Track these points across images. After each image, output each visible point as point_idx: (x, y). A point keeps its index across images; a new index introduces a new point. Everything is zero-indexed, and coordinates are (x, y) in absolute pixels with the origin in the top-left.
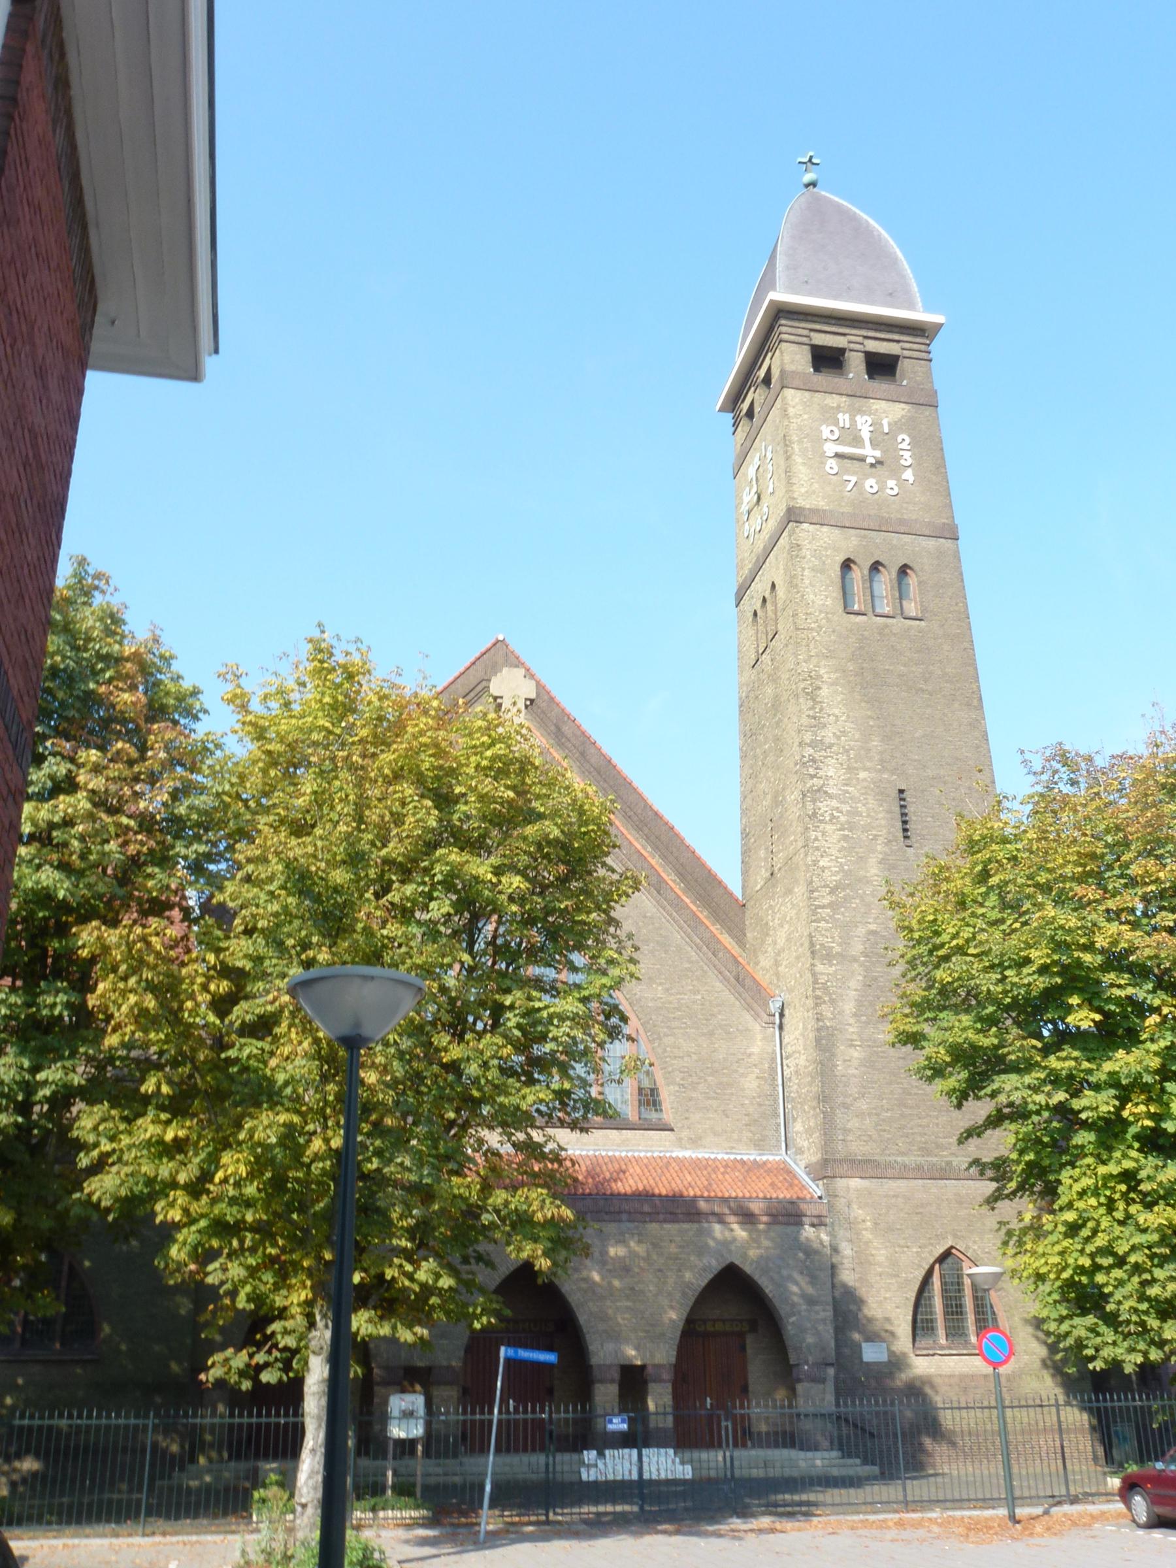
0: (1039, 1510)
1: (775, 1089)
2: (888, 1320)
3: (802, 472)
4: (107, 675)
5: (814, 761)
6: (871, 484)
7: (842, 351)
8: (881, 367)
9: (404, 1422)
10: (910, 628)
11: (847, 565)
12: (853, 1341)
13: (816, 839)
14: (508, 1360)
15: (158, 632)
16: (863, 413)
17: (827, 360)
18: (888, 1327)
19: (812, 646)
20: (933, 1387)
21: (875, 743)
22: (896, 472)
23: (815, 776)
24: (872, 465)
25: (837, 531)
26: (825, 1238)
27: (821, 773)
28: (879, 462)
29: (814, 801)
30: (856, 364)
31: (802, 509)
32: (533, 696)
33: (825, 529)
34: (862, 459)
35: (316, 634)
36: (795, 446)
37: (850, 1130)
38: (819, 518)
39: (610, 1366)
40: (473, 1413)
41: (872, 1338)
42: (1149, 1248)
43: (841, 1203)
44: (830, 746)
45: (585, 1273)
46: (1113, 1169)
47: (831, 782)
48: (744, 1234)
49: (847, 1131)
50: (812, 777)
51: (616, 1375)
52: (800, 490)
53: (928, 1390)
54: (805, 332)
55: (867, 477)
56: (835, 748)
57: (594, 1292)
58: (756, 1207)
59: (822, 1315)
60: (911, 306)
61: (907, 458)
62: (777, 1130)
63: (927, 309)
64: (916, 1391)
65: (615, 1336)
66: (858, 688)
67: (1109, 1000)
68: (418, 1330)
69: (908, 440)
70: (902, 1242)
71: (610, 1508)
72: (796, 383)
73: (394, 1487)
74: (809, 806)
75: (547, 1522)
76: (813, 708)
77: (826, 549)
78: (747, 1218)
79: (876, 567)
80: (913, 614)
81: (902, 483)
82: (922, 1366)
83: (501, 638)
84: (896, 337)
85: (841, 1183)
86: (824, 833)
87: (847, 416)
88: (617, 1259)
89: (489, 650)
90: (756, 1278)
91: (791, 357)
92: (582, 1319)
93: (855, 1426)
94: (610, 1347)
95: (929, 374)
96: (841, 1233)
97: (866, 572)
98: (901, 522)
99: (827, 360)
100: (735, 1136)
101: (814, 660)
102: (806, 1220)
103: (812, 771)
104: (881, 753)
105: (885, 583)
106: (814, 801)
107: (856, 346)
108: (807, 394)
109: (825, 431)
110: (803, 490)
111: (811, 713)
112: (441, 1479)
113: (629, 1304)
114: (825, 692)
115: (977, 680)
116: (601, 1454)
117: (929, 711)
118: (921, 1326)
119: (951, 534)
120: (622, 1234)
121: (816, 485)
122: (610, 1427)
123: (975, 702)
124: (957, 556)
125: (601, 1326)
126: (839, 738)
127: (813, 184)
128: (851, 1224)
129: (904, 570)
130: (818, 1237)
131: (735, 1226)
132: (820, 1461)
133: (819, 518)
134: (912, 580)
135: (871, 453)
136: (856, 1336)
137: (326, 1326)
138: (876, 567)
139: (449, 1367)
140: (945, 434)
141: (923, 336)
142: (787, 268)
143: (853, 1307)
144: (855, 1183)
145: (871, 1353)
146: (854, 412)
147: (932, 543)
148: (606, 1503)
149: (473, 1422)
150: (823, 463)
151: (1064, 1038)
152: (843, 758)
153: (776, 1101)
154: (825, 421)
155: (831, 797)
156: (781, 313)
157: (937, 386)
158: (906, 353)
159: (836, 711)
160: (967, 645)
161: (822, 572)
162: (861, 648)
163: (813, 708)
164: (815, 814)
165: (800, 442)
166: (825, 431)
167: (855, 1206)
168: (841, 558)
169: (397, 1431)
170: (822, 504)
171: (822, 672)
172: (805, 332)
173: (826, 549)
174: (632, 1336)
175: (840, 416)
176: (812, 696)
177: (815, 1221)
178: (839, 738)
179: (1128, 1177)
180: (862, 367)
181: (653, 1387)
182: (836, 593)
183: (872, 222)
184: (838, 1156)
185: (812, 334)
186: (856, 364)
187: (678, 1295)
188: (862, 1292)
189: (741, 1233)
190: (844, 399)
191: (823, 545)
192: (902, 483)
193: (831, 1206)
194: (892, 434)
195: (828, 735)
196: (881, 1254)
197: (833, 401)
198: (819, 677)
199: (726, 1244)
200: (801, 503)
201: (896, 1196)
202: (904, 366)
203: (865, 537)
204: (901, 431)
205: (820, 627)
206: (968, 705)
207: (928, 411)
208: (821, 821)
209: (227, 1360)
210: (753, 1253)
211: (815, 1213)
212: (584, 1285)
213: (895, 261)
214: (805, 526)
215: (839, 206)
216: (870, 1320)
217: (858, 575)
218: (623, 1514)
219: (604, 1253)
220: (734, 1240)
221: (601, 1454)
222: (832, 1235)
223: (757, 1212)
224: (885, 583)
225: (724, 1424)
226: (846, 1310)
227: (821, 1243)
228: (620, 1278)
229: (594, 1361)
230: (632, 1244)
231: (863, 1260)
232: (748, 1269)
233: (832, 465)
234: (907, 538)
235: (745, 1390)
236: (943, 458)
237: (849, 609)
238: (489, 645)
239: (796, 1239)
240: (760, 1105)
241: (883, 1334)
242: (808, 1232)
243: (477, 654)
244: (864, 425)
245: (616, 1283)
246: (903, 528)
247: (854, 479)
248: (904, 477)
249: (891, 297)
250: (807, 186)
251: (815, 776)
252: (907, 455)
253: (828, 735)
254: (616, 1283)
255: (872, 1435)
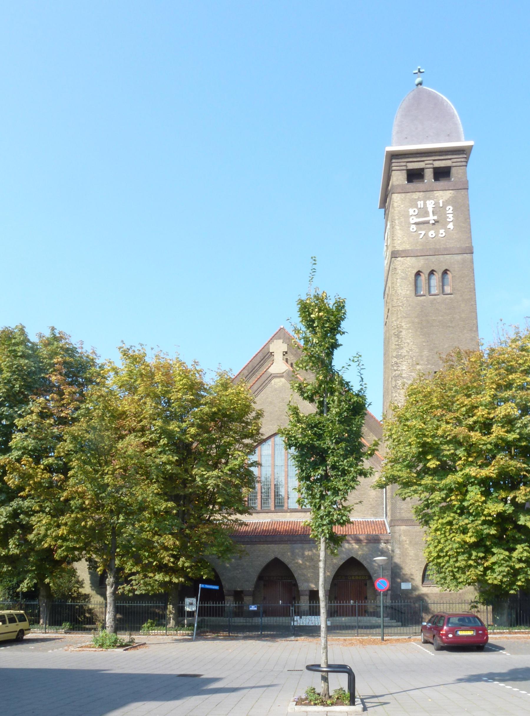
0: (407, 637)
1: (383, 494)
2: (412, 575)
3: (399, 233)
4: (50, 370)
5: (397, 364)
6: (432, 234)
7: (422, 170)
8: (442, 174)
9: (191, 606)
10: (446, 298)
11: (418, 274)
12: (397, 582)
13: (396, 396)
14: (201, 588)
15: (95, 349)
16: (429, 199)
17: (414, 176)
18: (412, 577)
19: (399, 313)
20: (428, 597)
21: (426, 353)
22: (444, 226)
23: (397, 370)
24: (433, 224)
25: (414, 259)
26: (390, 547)
27: (400, 368)
28: (436, 222)
29: (396, 381)
30: (429, 174)
31: (398, 251)
32: (286, 350)
33: (408, 258)
34: (428, 222)
35: (121, 345)
36: (397, 222)
37: (403, 509)
38: (405, 254)
39: (305, 591)
40: (205, 604)
41: (406, 581)
42: (456, 549)
43: (397, 535)
44: (405, 356)
45: (296, 561)
46: (444, 521)
47: (404, 372)
48: (357, 547)
49: (400, 509)
50: (395, 370)
51: (308, 593)
52: (397, 242)
53: (426, 598)
54: (404, 164)
55: (430, 230)
56: (407, 357)
57: (300, 567)
58: (361, 537)
59: (387, 573)
60: (459, 140)
61: (451, 217)
62: (383, 510)
63: (467, 139)
64: (421, 598)
65: (307, 581)
66: (419, 330)
67: (443, 456)
68: (180, 579)
69: (451, 208)
70: (421, 548)
71: (269, 633)
72: (399, 190)
73: (187, 625)
74: (394, 383)
75: (229, 636)
76: (397, 341)
77: (408, 268)
78: (358, 541)
79: (432, 272)
80: (449, 292)
81: (447, 230)
82: (424, 590)
83: (282, 327)
84: (449, 157)
85: (397, 528)
86: (399, 394)
87: (422, 202)
88: (308, 555)
89: (277, 332)
90: (361, 561)
91: (399, 178)
92: (296, 576)
93: (398, 611)
94: (306, 584)
95: (465, 173)
96: (396, 546)
97: (427, 276)
98: (446, 249)
99: (414, 176)
100: (366, 512)
101: (400, 320)
102: (382, 541)
103: (395, 368)
104: (428, 357)
105: (435, 280)
106: (396, 381)
107: (428, 165)
108: (403, 195)
109: (411, 211)
110: (399, 242)
111: (397, 343)
112: (245, 624)
113: (312, 571)
114: (404, 333)
115: (476, 318)
116: (301, 618)
117: (452, 335)
118: (424, 577)
119: (470, 251)
120: (311, 548)
121: (406, 239)
122: (251, 609)
123: (475, 329)
124: (472, 262)
125: (303, 578)
126: (408, 352)
127: (420, 84)
128: (400, 542)
129: (445, 272)
130: (387, 547)
131: (354, 544)
132: (379, 621)
133: (405, 254)
134: (450, 276)
135: (432, 218)
136: (399, 580)
137: (111, 578)
138: (432, 272)
139: (249, 591)
140: (471, 203)
141: (463, 154)
142: (398, 133)
143: (398, 571)
144: (403, 528)
145: (405, 586)
146: (425, 199)
147: (459, 257)
148: (269, 631)
149: (205, 607)
150: (409, 227)
151: (426, 471)
152: (410, 361)
153: (383, 499)
154: (412, 207)
155: (403, 378)
156: (394, 156)
157: (468, 178)
158: (454, 164)
159: (408, 341)
160: (473, 303)
161: (405, 279)
162: (422, 311)
163: (397, 341)
164: (396, 386)
165: (399, 218)
166: (411, 211)
167: (402, 536)
168: (415, 271)
169: (188, 609)
170: (407, 247)
171: (403, 324)
172: (404, 164)
173: (408, 268)
174: (314, 581)
175: (419, 203)
176: (398, 336)
177: (386, 541)
178: (408, 352)
179: (450, 523)
180: (432, 175)
181: (302, 598)
182: (412, 288)
183: (445, 98)
184: (397, 518)
185: (408, 164)
186: (429, 174)
187: (331, 568)
188: (403, 565)
189: (356, 546)
190: (421, 193)
191: (407, 266)
192: (447, 230)
193: (392, 537)
194: (444, 207)
195: (404, 352)
196: (411, 552)
197: (415, 196)
198: (402, 327)
199: (350, 550)
200: (399, 248)
201: (420, 532)
202: (453, 171)
203: (427, 259)
204: (449, 204)
205: (403, 304)
206: (471, 330)
207: (463, 192)
208: (398, 389)
209: (123, 588)
210: (360, 553)
211: (386, 539)
212: (296, 565)
213: (453, 116)
214: (399, 258)
215: (430, 92)
216: (404, 575)
217: (423, 278)
218: (273, 634)
219: (303, 554)
220: (353, 549)
221: (301, 618)
222: (392, 546)
223: (362, 539)
224: (435, 280)
225: (291, 608)
226: (395, 573)
227: (388, 549)
228: (310, 562)
229: (300, 589)
230: (314, 551)
231: (404, 554)
232: (358, 558)
233: (413, 228)
234: (448, 257)
235: (366, 598)
236: (469, 215)
237: (419, 294)
238: (277, 331)
239: (378, 548)
240: (376, 501)
241: (410, 580)
242: (383, 545)
243: (273, 335)
244: (430, 205)
245: (308, 564)
246: (447, 252)
247: (423, 232)
248: (448, 227)
249: (449, 137)
250: (417, 85)
251: (397, 370)
252: (450, 216)
253: (404, 352)
254: (308, 564)
255: (402, 613)
